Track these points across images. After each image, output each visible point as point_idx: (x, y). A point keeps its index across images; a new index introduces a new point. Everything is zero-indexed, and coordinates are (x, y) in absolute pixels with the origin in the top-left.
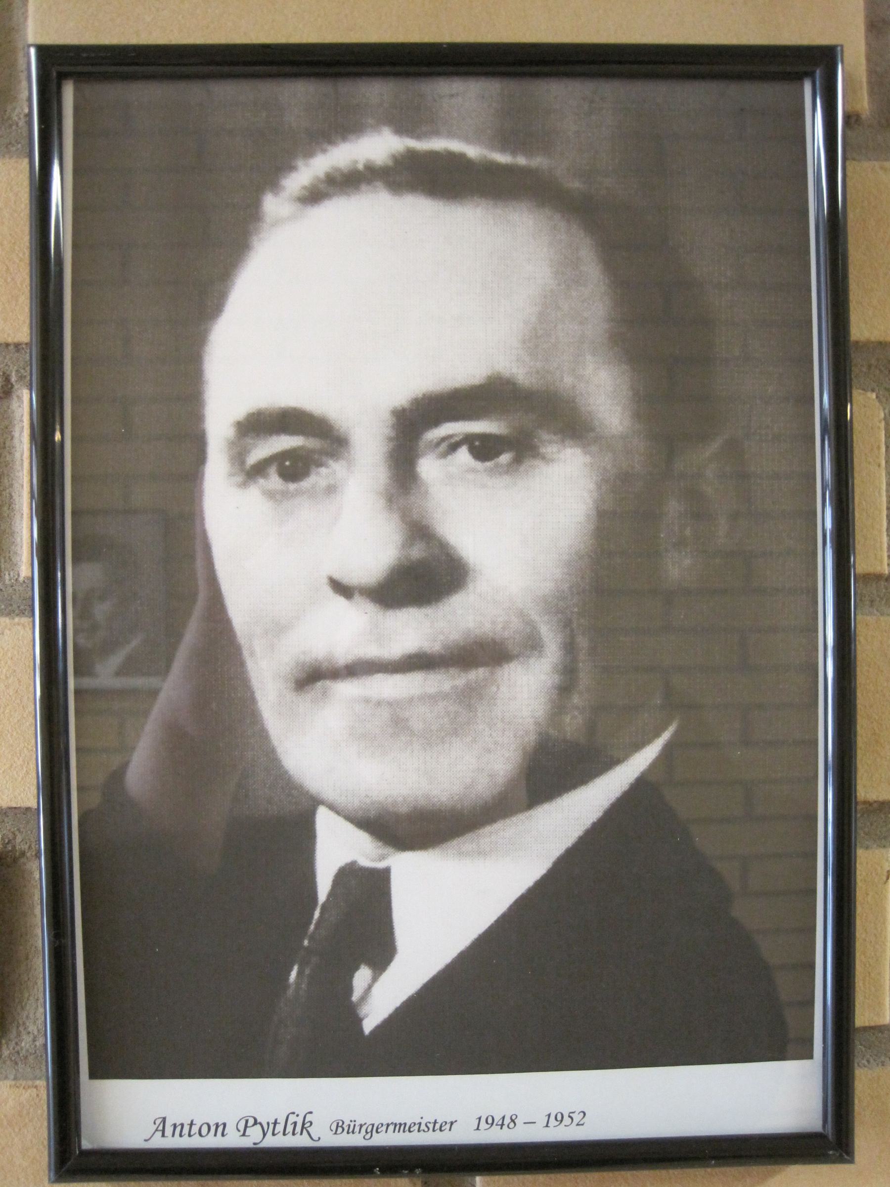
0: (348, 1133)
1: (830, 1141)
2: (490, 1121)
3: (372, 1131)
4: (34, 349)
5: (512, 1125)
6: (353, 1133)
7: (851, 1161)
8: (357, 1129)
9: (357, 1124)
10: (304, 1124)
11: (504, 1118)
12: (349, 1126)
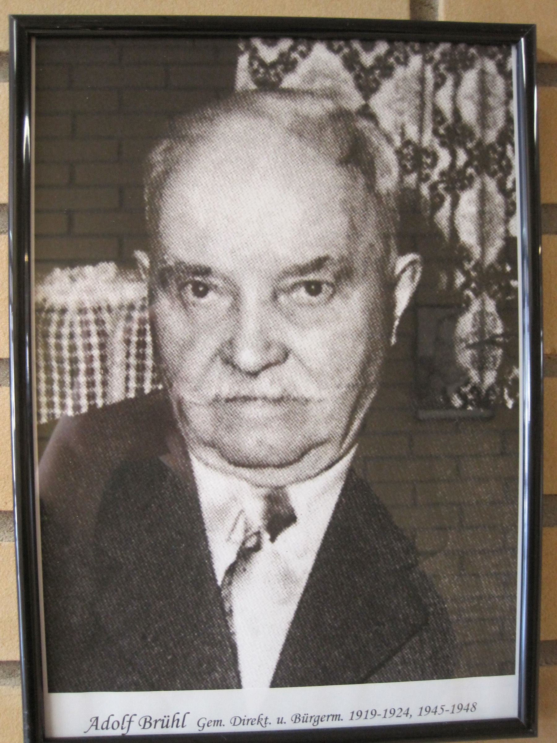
0: (303, 722)
1: (525, 723)
2: (428, 710)
3: (318, 721)
4: (11, 210)
5: (473, 709)
6: (167, 726)
7: (239, 686)
8: (309, 719)
9: (309, 716)
10: (259, 719)
11: (468, 705)
12: (304, 717)
